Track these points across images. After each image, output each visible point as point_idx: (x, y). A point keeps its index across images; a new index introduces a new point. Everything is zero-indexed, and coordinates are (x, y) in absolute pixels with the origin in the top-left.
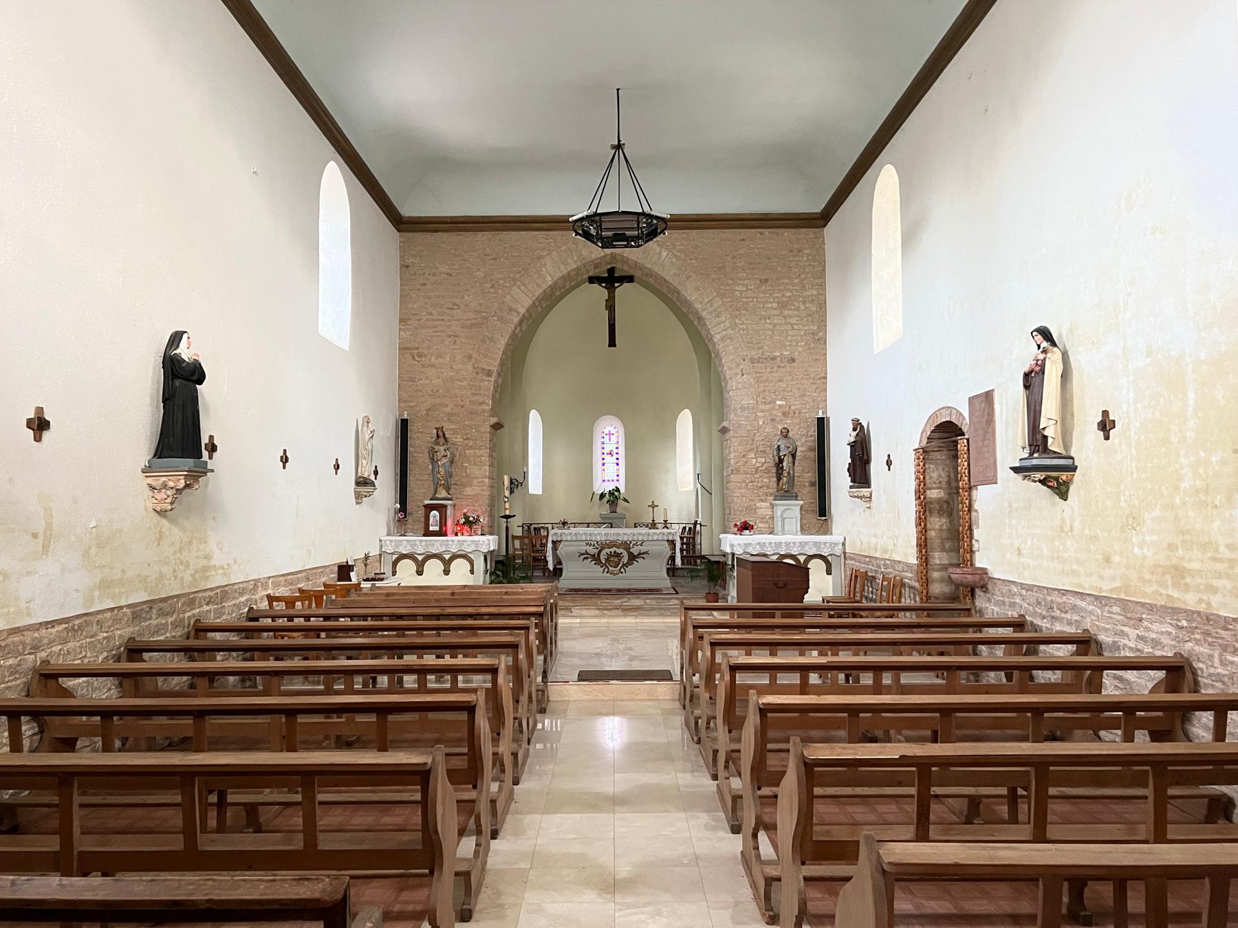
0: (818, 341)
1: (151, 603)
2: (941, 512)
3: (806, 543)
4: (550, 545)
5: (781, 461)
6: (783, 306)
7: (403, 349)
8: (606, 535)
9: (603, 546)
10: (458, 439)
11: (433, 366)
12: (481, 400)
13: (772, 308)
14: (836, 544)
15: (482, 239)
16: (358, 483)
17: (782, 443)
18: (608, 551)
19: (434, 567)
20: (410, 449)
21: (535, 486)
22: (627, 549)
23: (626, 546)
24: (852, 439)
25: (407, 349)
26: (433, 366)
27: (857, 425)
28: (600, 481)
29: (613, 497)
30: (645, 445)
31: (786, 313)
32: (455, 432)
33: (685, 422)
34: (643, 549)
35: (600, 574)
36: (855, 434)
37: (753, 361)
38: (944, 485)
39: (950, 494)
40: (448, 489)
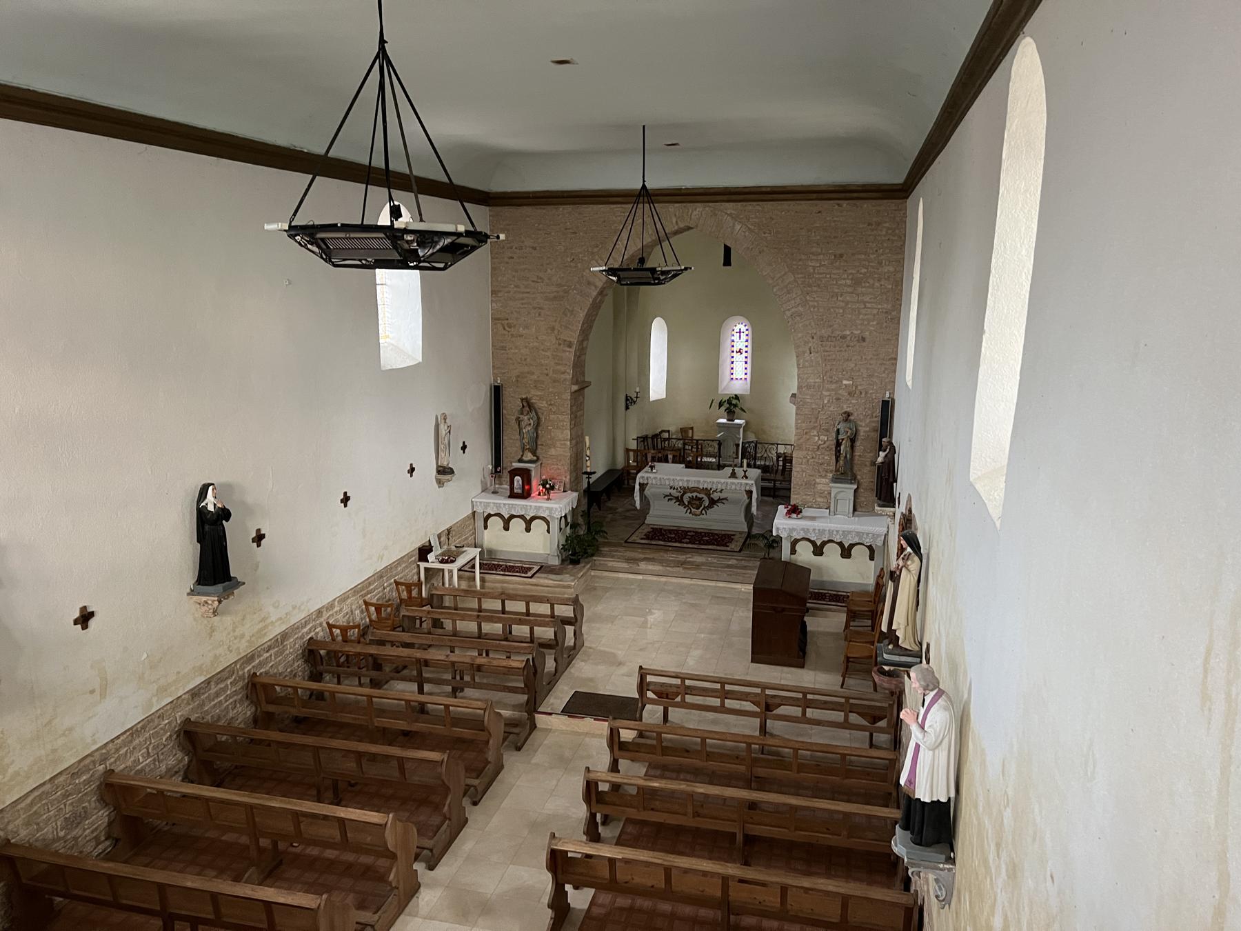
1: (208, 682)
3: (850, 532)
4: (637, 487)
5: (838, 444)
6: (857, 282)
9: (685, 490)
10: (543, 404)
11: (521, 336)
13: (846, 285)
14: (879, 536)
15: (564, 213)
16: (439, 472)
17: (842, 426)
19: (517, 525)
21: (657, 388)
22: (708, 495)
23: (707, 492)
26: (521, 336)
28: (728, 376)
29: (732, 405)
31: (860, 290)
32: (541, 398)
34: (723, 495)
35: (683, 514)
40: (534, 453)
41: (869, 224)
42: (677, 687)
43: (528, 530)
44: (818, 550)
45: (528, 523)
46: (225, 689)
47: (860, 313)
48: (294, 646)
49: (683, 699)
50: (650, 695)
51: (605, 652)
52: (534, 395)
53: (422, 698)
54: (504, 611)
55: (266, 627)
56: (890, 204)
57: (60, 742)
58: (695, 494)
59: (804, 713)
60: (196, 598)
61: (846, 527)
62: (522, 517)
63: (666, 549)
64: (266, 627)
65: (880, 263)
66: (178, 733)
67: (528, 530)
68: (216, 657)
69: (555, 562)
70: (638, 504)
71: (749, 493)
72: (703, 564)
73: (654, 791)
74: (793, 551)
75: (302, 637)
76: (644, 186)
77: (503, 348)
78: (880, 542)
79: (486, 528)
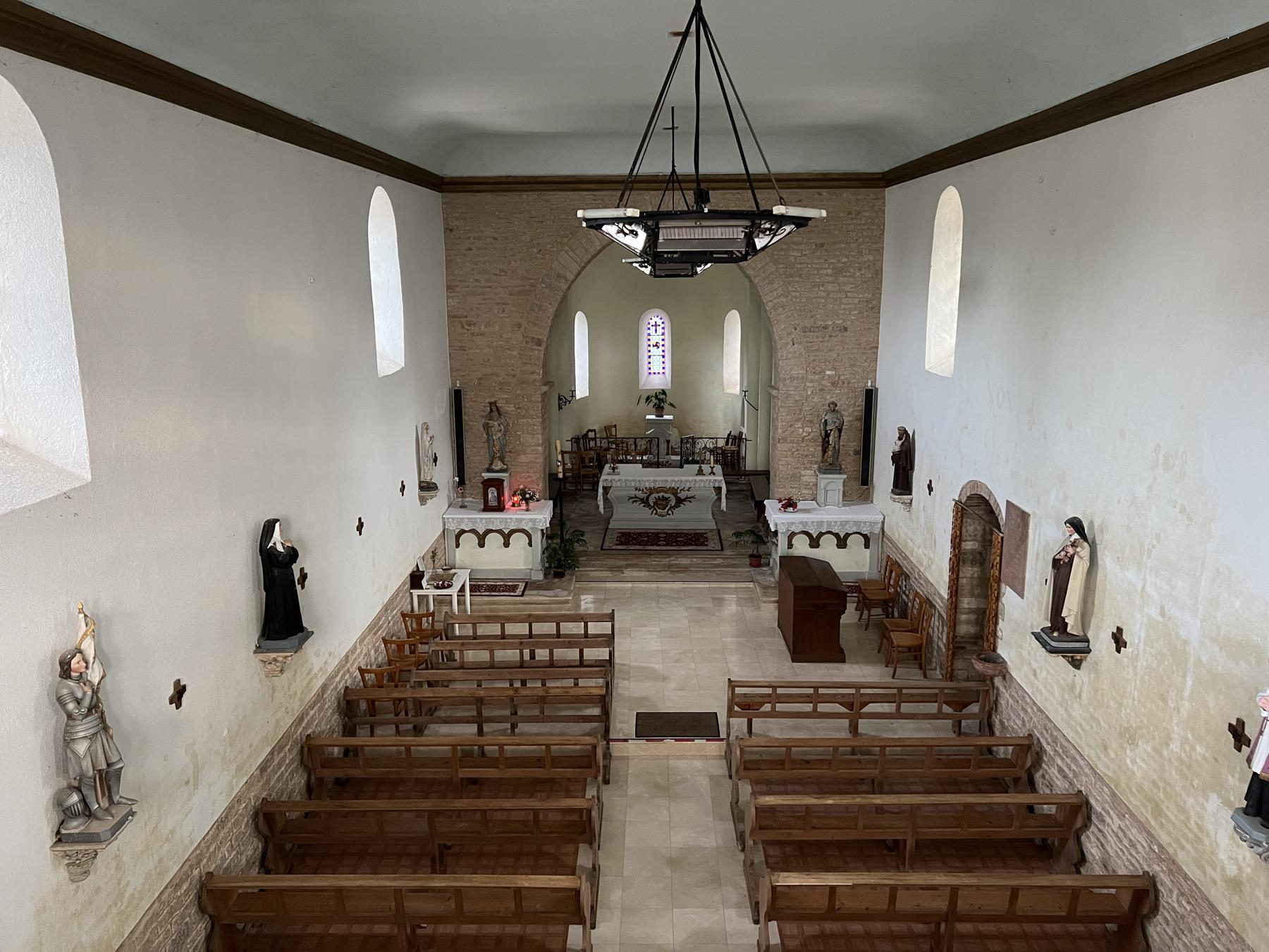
0: (872, 309)
1: (272, 753)
2: (973, 562)
3: (847, 522)
4: (601, 491)
5: (827, 435)
6: (838, 272)
7: (452, 317)
8: (655, 481)
9: (651, 491)
10: (511, 408)
11: (483, 334)
12: (532, 369)
13: (827, 275)
14: (876, 523)
16: (421, 488)
18: (656, 495)
19: (494, 540)
20: (465, 418)
23: (674, 491)
24: (897, 449)
25: (455, 317)
26: (483, 334)
27: (903, 433)
29: (659, 400)
30: (692, 345)
31: (841, 279)
32: (507, 401)
33: (733, 326)
34: (690, 494)
36: (900, 443)
37: (805, 330)
38: (979, 538)
39: (984, 546)
40: (502, 459)
41: (850, 213)
42: (770, 695)
43: (507, 545)
44: (815, 543)
45: (507, 538)
46: (284, 758)
47: (841, 303)
48: (331, 698)
49: (773, 708)
50: (736, 708)
51: (641, 668)
52: (501, 398)
53: (482, 740)
54: (531, 636)
55: (312, 680)
56: (866, 194)
57: (166, 847)
58: (661, 495)
59: (815, 708)
60: (261, 656)
61: (844, 517)
62: (500, 532)
63: (648, 554)
64: (312, 680)
65: (860, 252)
66: (255, 816)
67: (507, 545)
68: (277, 722)
69: (540, 576)
70: (601, 509)
71: (718, 489)
72: (691, 566)
73: (772, 810)
74: (790, 546)
75: (336, 688)
76: (674, 171)
77: (463, 348)
78: (877, 530)
79: (458, 546)
